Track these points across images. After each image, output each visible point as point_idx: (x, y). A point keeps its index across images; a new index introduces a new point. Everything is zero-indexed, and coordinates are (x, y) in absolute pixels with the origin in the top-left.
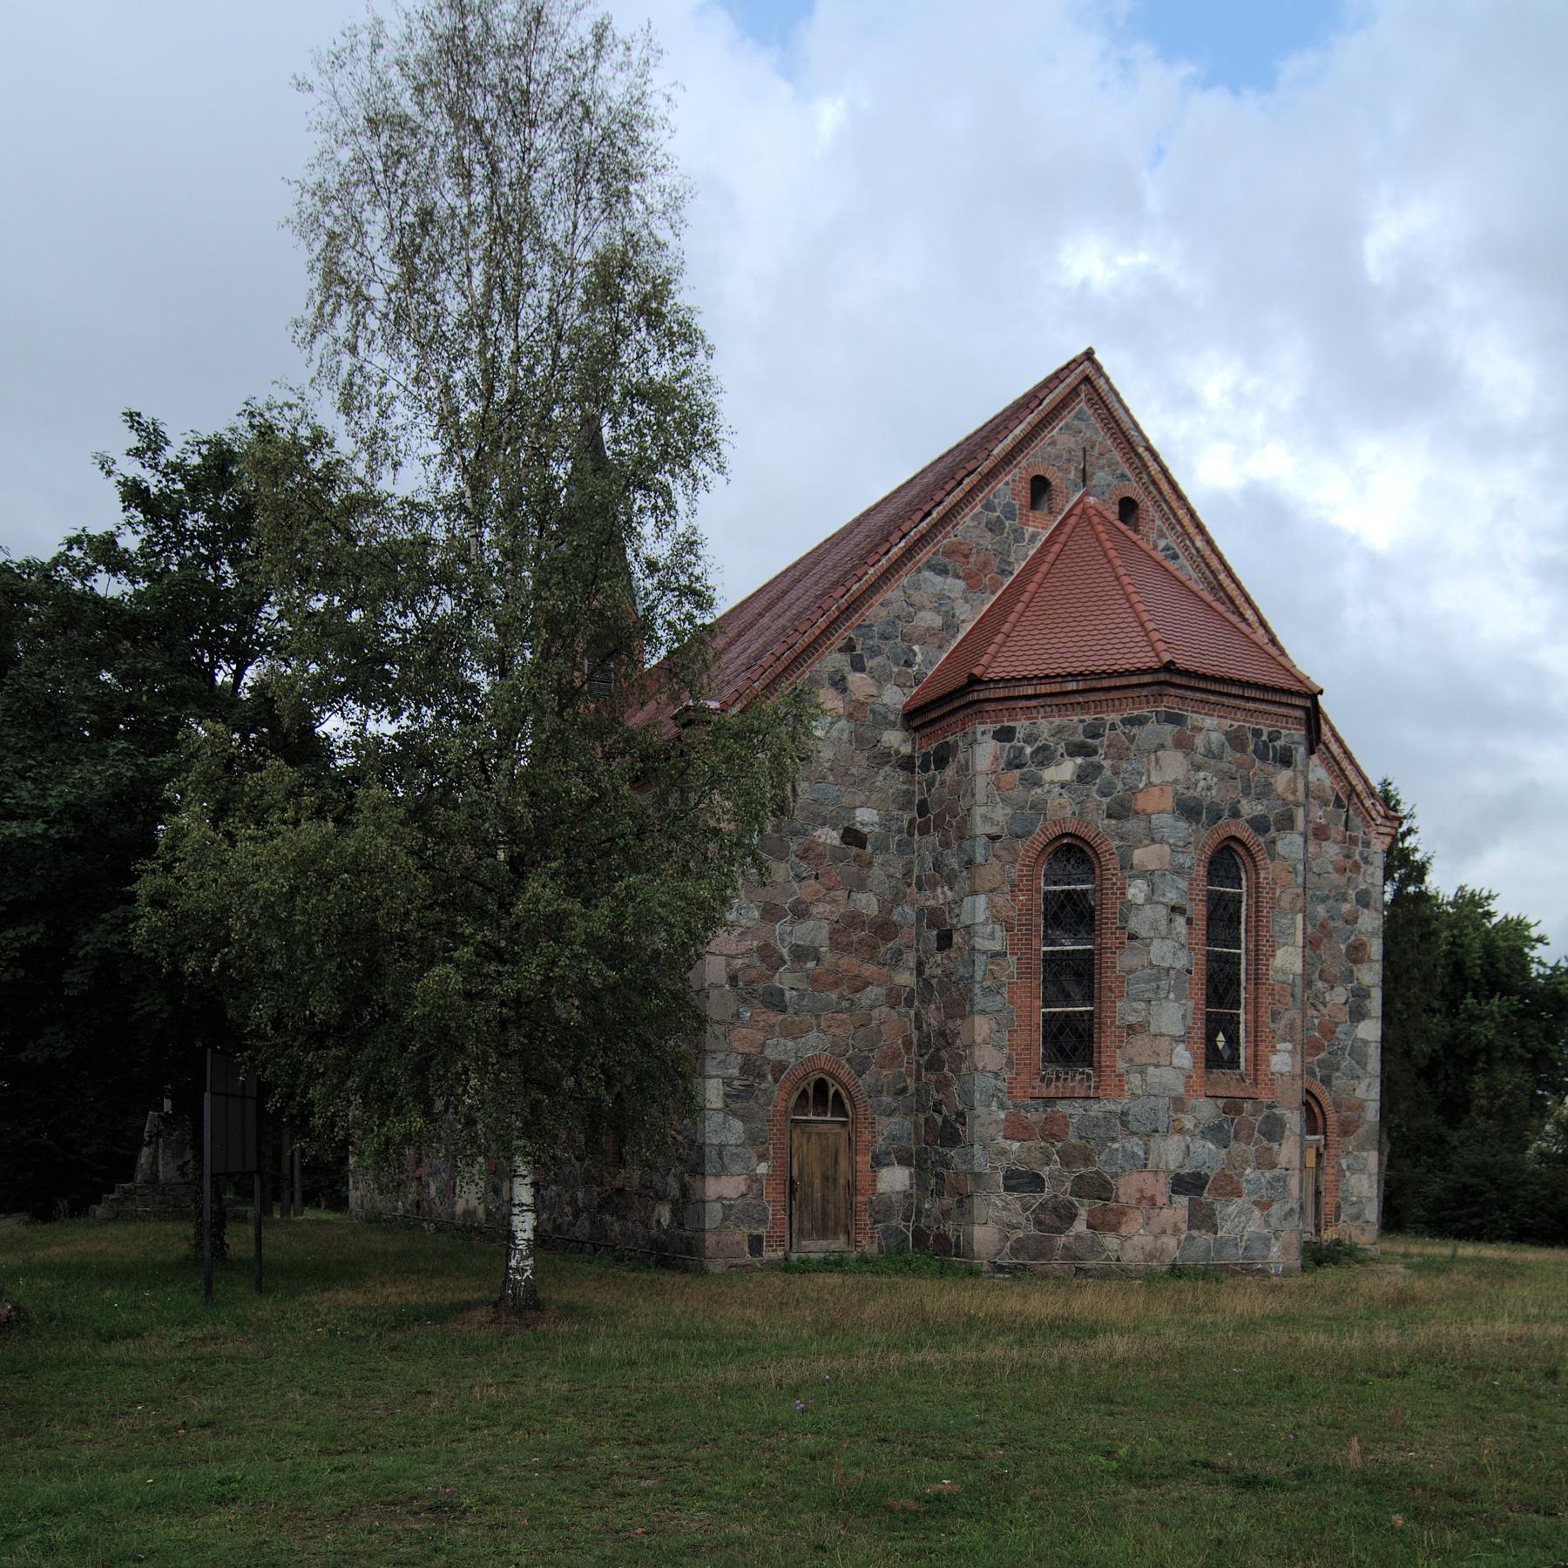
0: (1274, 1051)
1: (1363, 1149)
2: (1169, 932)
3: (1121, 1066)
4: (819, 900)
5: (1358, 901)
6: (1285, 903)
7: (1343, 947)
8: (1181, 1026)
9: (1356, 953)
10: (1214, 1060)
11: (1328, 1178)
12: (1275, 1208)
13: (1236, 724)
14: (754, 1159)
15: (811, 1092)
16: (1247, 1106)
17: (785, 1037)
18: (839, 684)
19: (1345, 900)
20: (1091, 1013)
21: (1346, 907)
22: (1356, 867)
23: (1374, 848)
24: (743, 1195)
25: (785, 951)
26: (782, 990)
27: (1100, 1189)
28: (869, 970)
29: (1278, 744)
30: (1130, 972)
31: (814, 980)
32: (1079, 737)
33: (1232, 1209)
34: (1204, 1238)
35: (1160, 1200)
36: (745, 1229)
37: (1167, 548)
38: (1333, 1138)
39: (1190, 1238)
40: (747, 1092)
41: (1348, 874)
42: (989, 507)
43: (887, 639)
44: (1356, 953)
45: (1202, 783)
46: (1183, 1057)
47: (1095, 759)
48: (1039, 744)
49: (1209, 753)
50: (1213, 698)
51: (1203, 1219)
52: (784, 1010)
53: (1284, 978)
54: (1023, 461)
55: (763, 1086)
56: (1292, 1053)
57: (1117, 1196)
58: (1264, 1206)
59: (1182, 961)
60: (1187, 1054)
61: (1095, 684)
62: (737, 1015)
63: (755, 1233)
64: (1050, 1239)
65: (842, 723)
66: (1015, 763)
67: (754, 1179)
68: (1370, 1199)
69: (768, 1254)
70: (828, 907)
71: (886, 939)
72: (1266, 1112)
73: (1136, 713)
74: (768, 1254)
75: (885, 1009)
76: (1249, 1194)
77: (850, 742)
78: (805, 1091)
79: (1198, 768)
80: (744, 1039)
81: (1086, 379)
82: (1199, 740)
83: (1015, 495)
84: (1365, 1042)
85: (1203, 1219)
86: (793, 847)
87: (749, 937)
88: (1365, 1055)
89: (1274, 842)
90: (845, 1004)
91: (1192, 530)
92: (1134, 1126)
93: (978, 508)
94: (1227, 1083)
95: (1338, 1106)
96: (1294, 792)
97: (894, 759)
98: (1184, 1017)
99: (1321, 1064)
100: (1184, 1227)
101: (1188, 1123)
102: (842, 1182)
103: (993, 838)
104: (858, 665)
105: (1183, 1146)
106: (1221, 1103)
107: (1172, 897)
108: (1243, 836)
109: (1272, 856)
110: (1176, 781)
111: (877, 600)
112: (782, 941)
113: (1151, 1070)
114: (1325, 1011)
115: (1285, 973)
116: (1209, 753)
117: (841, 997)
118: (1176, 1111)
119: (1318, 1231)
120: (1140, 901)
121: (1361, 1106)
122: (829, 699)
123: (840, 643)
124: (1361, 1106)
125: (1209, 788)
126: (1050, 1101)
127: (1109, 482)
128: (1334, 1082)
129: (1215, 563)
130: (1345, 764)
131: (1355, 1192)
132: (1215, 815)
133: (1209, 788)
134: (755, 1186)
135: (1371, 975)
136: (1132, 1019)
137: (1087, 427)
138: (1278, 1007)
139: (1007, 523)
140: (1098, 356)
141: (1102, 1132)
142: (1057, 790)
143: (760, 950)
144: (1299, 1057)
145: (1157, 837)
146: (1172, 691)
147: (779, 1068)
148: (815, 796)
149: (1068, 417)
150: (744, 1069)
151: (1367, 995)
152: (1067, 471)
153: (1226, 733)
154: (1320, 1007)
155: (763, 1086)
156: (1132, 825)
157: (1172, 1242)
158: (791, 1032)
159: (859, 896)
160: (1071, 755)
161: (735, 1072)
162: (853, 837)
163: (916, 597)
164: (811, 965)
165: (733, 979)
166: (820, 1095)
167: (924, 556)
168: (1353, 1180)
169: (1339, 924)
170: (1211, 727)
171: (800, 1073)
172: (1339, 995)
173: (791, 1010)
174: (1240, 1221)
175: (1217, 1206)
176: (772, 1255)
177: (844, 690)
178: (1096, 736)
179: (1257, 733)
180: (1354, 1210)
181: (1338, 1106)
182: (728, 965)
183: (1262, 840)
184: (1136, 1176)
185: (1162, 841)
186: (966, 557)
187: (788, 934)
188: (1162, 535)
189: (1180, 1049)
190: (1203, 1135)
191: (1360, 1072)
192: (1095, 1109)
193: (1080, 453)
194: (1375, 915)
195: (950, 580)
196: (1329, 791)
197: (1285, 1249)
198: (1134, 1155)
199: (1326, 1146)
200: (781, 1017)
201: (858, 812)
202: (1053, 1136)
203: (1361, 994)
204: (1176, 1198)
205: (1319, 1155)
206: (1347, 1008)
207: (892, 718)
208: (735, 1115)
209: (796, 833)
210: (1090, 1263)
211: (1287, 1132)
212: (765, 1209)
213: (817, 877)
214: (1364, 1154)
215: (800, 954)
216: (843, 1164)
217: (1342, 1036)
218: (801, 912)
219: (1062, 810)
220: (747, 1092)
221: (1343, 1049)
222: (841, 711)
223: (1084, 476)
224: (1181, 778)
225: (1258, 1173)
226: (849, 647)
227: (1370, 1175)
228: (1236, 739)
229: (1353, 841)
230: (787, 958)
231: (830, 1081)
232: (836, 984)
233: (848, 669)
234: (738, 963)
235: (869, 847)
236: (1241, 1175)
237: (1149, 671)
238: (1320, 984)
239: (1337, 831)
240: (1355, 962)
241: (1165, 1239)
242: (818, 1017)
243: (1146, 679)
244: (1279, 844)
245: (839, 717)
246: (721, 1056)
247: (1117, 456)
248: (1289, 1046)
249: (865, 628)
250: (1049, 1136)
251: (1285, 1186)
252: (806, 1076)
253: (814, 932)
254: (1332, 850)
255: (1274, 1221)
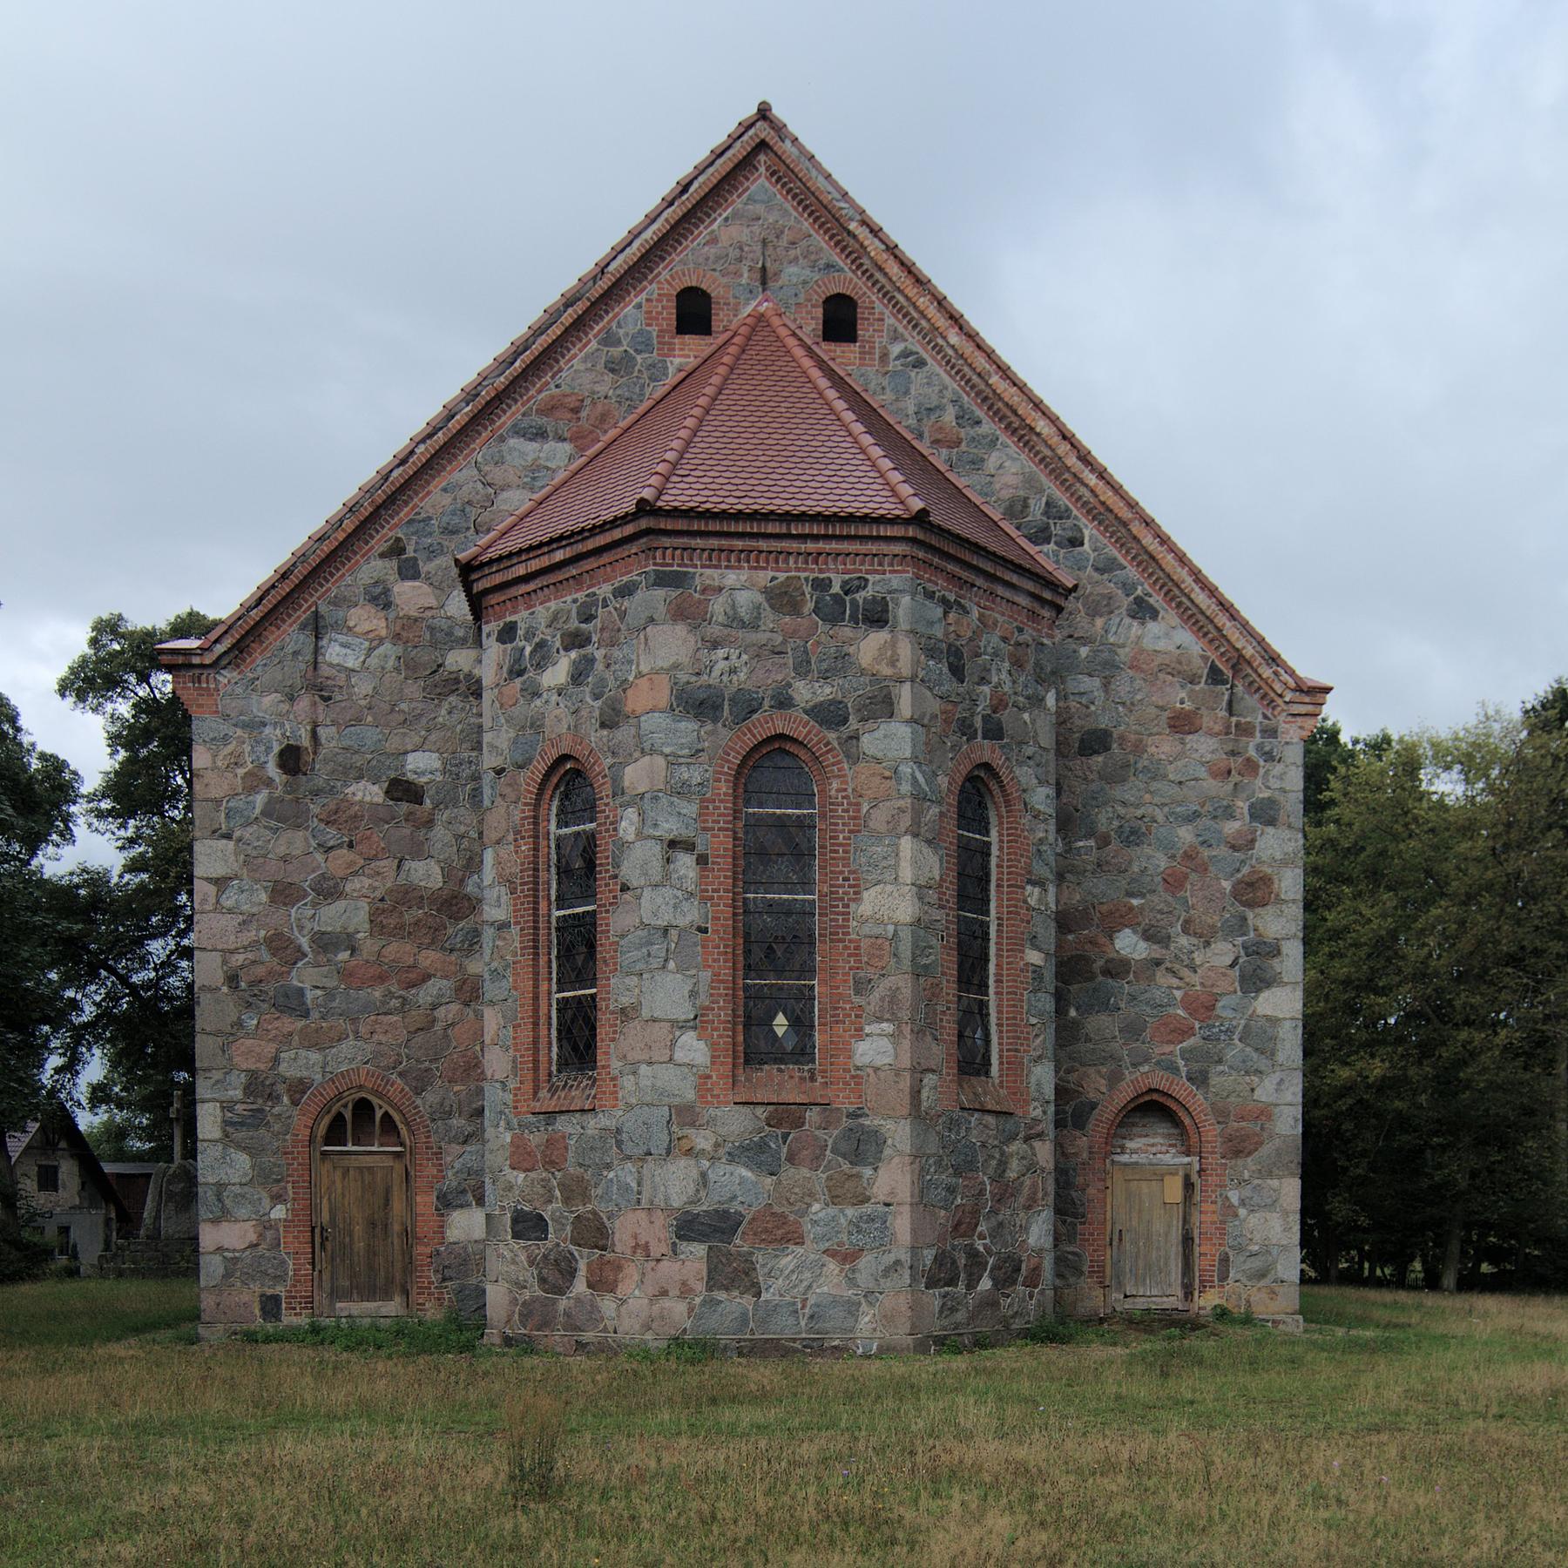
0: (860, 1035)
1: (1270, 1175)
2: (667, 876)
3: (616, 1065)
4: (354, 874)
5: (1253, 817)
6: (879, 820)
7: (1227, 885)
8: (687, 1005)
9: (1254, 891)
10: (753, 1047)
11: (1205, 1217)
12: (866, 1262)
13: (782, 576)
14: (266, 1202)
15: (348, 1115)
16: (812, 1115)
17: (308, 1048)
18: (381, 599)
19: (1232, 817)
20: (593, 996)
21: (1231, 827)
22: (1251, 767)
23: (1283, 738)
24: (253, 1246)
25: (304, 942)
26: (302, 989)
27: (594, 1234)
28: (429, 958)
29: (860, 596)
30: (622, 936)
31: (345, 974)
32: (574, 624)
33: (788, 1262)
34: (735, 1303)
35: (656, 1251)
36: (256, 1288)
37: (905, 354)
38: (1212, 1160)
39: (711, 1303)
40: (257, 1119)
41: (1235, 778)
42: (609, 340)
43: (453, 533)
44: (1254, 891)
45: (722, 665)
46: (694, 1049)
47: (589, 649)
48: (537, 640)
49: (734, 621)
50: (739, 544)
51: (731, 1274)
52: (306, 1014)
53: (878, 930)
54: (663, 272)
55: (276, 1110)
56: (895, 1037)
57: (613, 1244)
58: (848, 1257)
59: (691, 914)
60: (702, 1045)
61: (581, 548)
62: (239, 1024)
63: (270, 1292)
64: (554, 1302)
65: (387, 647)
66: (516, 672)
67: (266, 1225)
68: (1285, 1248)
69: (288, 1319)
70: (367, 882)
71: (457, 918)
72: (845, 1122)
73: (625, 579)
74: (288, 1319)
75: (455, 1007)
76: (816, 1240)
77: (397, 670)
78: (339, 1117)
79: (715, 645)
80: (251, 1053)
81: (762, 145)
82: (718, 606)
83: (650, 318)
84: (1274, 1021)
85: (731, 1274)
86: (315, 809)
87: (254, 925)
88: (1274, 1039)
89: (855, 737)
90: (395, 1003)
91: (941, 322)
92: (629, 1148)
93: (594, 345)
94: (782, 1083)
95: (1222, 1115)
96: (893, 662)
97: (463, 687)
98: (693, 994)
99: (1187, 1055)
100: (700, 1287)
101: (703, 1140)
102: (397, 1228)
103: (499, 772)
104: (409, 571)
105: (695, 1173)
106: (759, 1110)
107: (670, 827)
108: (800, 733)
109: (854, 759)
110: (676, 666)
111: (437, 485)
112: (301, 928)
113: (644, 1069)
114: (1195, 979)
115: (880, 923)
116: (734, 621)
117: (390, 994)
118: (682, 1125)
119: (1188, 1294)
120: (631, 838)
121: (1265, 1113)
122: (365, 619)
123: (384, 547)
124: (1265, 1113)
125: (733, 671)
126: (551, 1115)
127: (804, 280)
128: (1214, 1080)
129: (981, 362)
130: (1222, 620)
131: (1257, 1237)
132: (747, 707)
133: (733, 671)
134: (269, 1234)
135: (1282, 923)
136: (625, 1001)
137: (770, 209)
138: (871, 973)
139: (639, 358)
140: (778, 111)
141: (596, 1157)
142: (555, 698)
143: (269, 941)
144: (906, 1044)
145: (647, 746)
146: (666, 541)
147: (299, 1088)
148: (345, 743)
149: (737, 203)
150: (249, 1090)
151: (1275, 951)
152: (738, 274)
153: (766, 591)
154: (1185, 972)
155: (276, 1110)
156: (624, 734)
157: (680, 1308)
158: (314, 1041)
159: (414, 864)
160: (567, 649)
161: (238, 1094)
162: (404, 790)
163: (496, 475)
164: (344, 956)
165: (232, 979)
166: (355, 1119)
167: (507, 418)
168: (1253, 1220)
169: (1222, 851)
170: (738, 586)
171: (330, 1092)
172: (1223, 953)
173: (315, 1015)
174: (800, 1280)
175: (759, 1258)
176: (295, 1320)
177: (387, 606)
178: (588, 619)
179: (821, 585)
180: (1256, 1264)
181: (1222, 1115)
182: (225, 962)
183: (832, 736)
184: (630, 1215)
185: (653, 751)
186: (576, 411)
187: (304, 922)
188: (896, 337)
189: (689, 1038)
190: (732, 1158)
191: (1263, 1064)
192: (593, 1124)
193: (758, 248)
194: (1287, 834)
195: (551, 445)
196: (1198, 662)
197: (888, 1319)
198: (627, 1188)
199: (1201, 1171)
200: (301, 1024)
201: (410, 758)
202: (552, 1163)
203: (1263, 951)
204: (684, 1246)
205: (1188, 1185)
206: (1236, 971)
207: (460, 633)
208: (240, 1147)
209: (316, 793)
210: (588, 1336)
211: (887, 1152)
212: (284, 1262)
213: (351, 845)
214: (1275, 1183)
215: (325, 943)
216: (398, 1205)
217: (1228, 1014)
218: (329, 891)
219: (558, 719)
220: (257, 1119)
221: (1230, 1032)
222: (383, 633)
223: (764, 277)
224: (685, 660)
225: (832, 1210)
226: (397, 550)
227: (1286, 1213)
228: (783, 599)
229: (1245, 730)
230: (306, 948)
231: (375, 1101)
232: (382, 978)
233: (393, 576)
234: (239, 959)
235: (428, 803)
236: (804, 1213)
237: (895, 521)
238: (1184, 941)
239: (1215, 717)
240: (1250, 905)
241: (666, 1303)
242: (354, 1021)
243: (629, 529)
244: (865, 739)
245: (381, 641)
246: (217, 1075)
247: (820, 240)
248: (887, 1027)
249: (420, 524)
250: (551, 1164)
251: (884, 1227)
252: (339, 1097)
253: (349, 914)
254: (1204, 746)
255: (864, 1279)
